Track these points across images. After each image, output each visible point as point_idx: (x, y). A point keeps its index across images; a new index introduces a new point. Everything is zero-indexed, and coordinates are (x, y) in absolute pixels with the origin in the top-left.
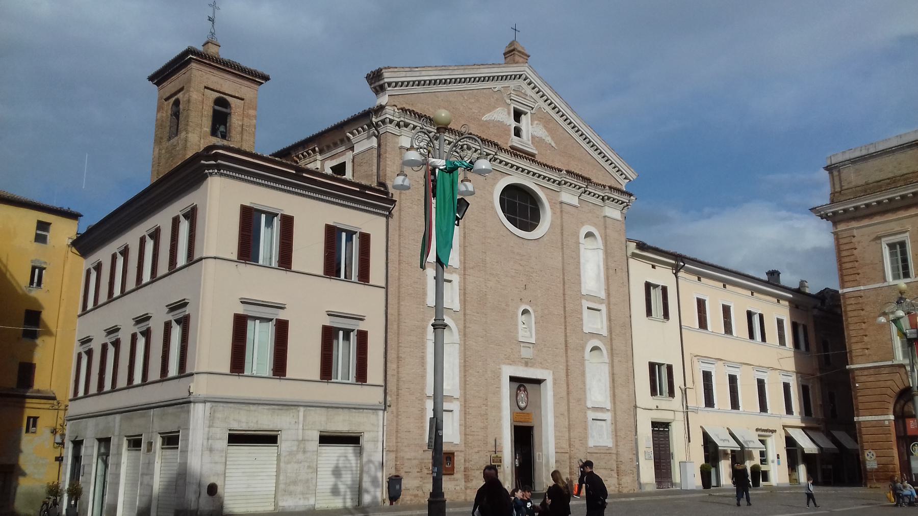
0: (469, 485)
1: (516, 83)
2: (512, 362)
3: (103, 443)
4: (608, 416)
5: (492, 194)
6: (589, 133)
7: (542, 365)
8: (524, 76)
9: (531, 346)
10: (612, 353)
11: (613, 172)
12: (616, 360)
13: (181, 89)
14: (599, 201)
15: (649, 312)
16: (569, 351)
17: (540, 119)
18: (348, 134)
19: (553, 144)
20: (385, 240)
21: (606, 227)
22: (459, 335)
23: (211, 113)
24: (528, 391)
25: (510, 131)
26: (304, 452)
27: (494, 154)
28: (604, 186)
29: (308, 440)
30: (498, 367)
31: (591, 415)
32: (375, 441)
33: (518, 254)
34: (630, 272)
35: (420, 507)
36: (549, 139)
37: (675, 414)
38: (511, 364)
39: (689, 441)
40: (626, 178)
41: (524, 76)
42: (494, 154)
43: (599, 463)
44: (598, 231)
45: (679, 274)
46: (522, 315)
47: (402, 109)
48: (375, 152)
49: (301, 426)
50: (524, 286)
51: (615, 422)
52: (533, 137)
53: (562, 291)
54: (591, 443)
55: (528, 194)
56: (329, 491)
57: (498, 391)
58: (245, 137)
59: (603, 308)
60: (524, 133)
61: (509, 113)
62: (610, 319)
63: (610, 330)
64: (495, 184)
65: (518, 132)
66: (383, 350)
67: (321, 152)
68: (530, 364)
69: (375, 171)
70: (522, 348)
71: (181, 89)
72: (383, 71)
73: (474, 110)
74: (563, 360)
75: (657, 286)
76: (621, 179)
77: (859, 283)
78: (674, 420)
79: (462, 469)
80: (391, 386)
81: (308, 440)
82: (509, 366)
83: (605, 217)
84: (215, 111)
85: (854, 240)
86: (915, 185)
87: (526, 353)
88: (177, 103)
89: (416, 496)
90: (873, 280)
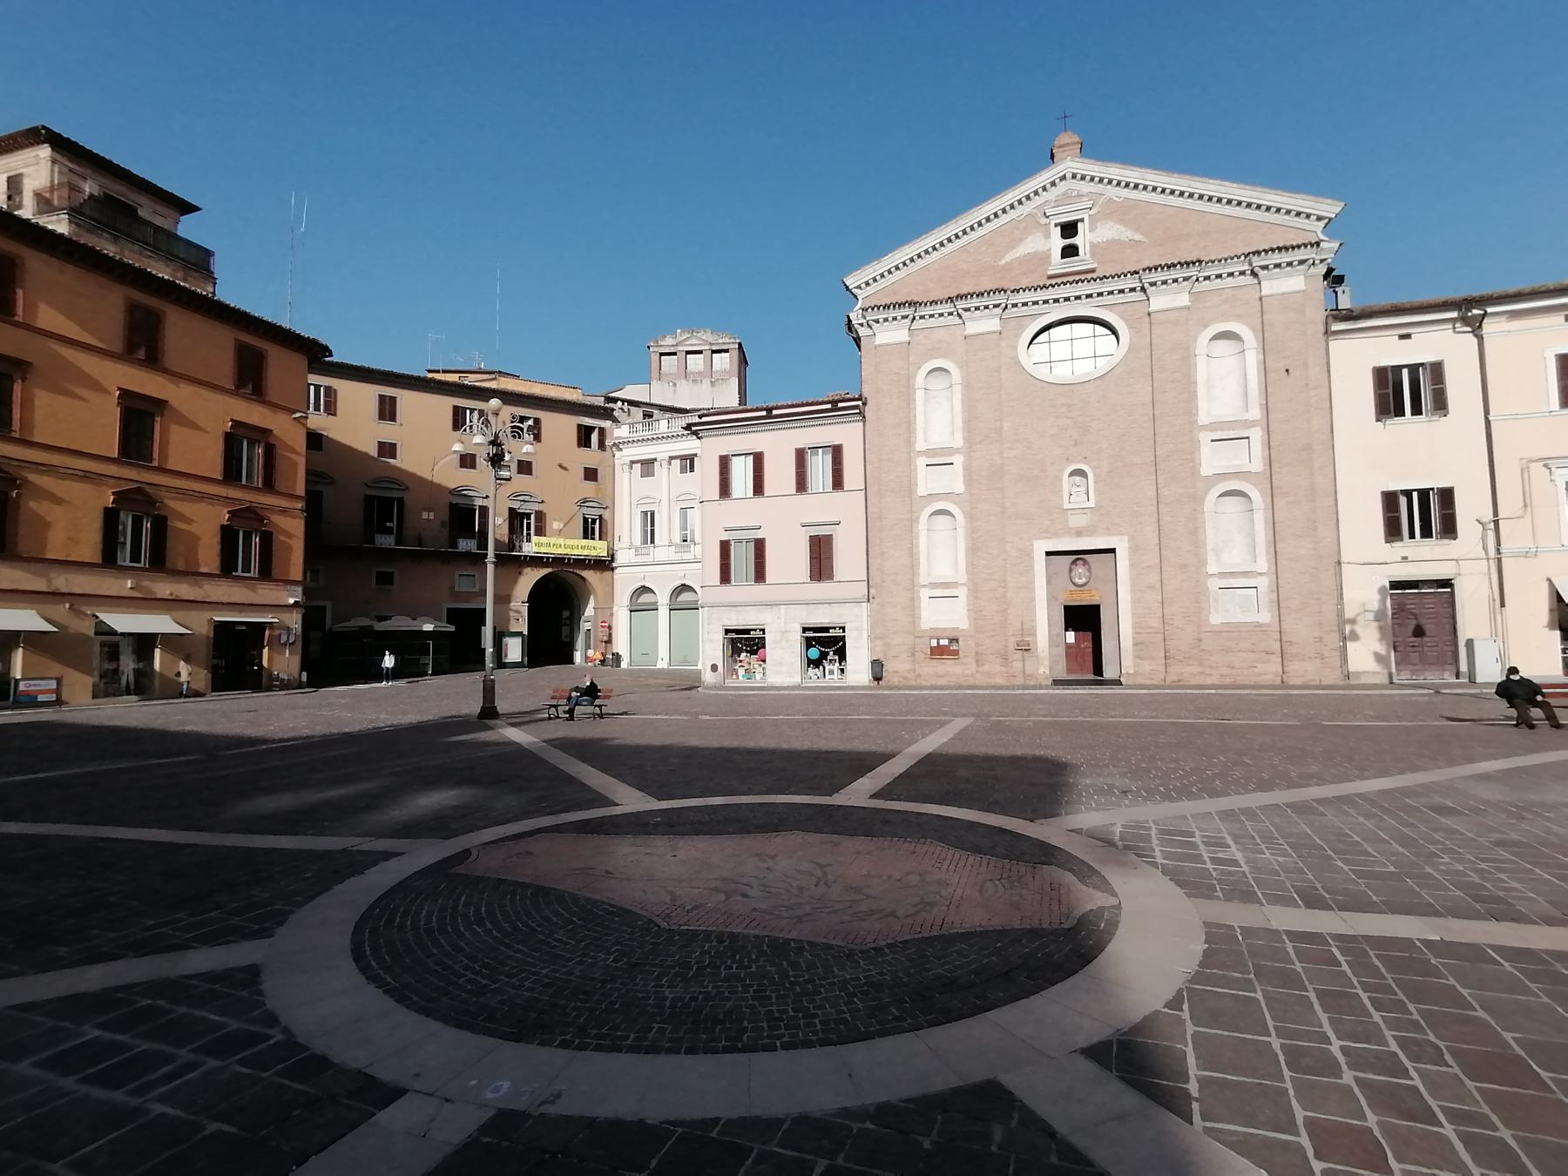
0: (981, 669)
2: (1047, 534)
6: (16, 717)
7: (1109, 532)
11: (1291, 220)
22: (965, 518)
24: (1091, 564)
26: (787, 641)
27: (1005, 301)
29: (790, 631)
30: (1028, 544)
31: (1214, 584)
32: (859, 629)
33: (1063, 405)
37: (1458, 564)
38: (1050, 538)
39: (1503, 605)
42: (1005, 301)
44: (1244, 324)
46: (1069, 476)
49: (783, 621)
50: (1074, 443)
54: (1216, 619)
57: (1030, 569)
64: (1019, 335)
65: (1070, 251)
70: (1069, 516)
73: (985, 260)
74: (1154, 519)
79: (974, 654)
81: (790, 631)
86: (132, 706)
87: (1076, 521)
89: (906, 678)
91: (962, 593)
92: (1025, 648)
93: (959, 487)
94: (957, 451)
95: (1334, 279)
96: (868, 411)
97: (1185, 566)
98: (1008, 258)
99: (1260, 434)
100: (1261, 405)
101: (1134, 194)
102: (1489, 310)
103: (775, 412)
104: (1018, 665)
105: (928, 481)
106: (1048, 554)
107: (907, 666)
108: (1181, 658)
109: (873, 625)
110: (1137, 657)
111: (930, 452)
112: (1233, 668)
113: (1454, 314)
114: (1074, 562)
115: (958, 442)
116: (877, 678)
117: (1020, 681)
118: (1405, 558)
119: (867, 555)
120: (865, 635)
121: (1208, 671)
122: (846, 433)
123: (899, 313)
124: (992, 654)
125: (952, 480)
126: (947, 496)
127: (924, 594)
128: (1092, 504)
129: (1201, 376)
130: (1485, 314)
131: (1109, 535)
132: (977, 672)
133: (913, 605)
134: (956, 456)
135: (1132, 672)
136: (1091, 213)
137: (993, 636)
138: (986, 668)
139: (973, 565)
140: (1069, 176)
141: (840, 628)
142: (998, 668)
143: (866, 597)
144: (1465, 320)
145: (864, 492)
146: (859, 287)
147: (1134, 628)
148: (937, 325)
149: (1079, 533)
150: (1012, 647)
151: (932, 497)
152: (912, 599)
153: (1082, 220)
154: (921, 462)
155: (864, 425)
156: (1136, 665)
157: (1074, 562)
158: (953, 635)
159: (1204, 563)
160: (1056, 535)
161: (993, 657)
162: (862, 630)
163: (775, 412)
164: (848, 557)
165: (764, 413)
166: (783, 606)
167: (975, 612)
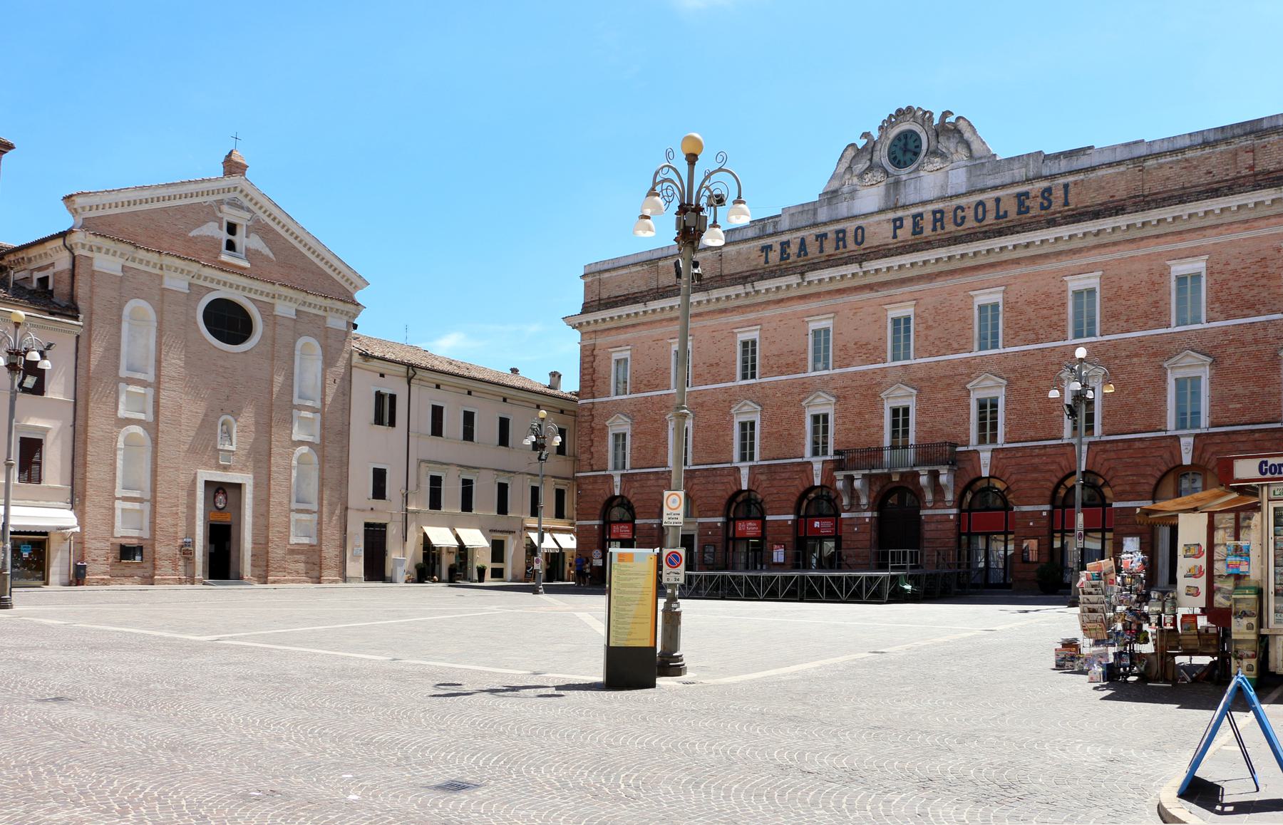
8: (239, 189)
12: (327, 466)
25: (220, 244)
33: (222, 366)
34: (353, 380)
35: (1218, 560)
36: (266, 251)
41: (239, 189)
56: (868, 543)
61: (221, 228)
63: (323, 438)
98: (193, 234)
146: (83, 208)
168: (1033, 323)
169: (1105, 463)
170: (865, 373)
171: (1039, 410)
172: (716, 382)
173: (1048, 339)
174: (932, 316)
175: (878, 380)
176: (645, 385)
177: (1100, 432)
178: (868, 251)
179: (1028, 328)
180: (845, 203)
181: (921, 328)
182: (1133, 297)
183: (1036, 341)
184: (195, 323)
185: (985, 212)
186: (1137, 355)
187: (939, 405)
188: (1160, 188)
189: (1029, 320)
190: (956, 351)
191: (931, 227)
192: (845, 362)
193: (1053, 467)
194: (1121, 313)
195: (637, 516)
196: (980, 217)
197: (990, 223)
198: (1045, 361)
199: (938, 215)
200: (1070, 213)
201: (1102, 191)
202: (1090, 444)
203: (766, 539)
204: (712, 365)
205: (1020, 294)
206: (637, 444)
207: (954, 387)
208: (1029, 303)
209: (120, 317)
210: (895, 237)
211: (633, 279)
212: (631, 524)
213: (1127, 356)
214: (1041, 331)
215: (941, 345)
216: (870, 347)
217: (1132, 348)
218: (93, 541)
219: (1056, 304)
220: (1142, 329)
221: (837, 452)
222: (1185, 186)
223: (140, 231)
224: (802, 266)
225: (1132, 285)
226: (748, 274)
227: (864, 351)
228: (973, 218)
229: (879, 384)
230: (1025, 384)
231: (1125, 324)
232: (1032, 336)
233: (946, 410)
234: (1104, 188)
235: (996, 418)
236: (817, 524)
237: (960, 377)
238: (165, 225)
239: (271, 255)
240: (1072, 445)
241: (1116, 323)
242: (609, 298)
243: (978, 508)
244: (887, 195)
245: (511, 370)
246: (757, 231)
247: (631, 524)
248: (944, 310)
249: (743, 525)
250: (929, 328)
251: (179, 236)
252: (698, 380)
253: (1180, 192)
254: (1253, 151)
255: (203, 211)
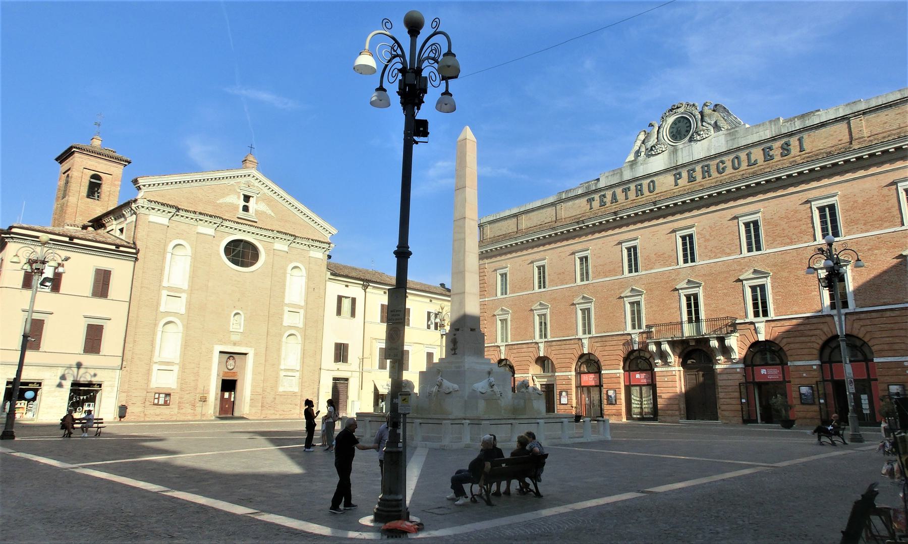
0: (181, 411)
1: (247, 179)
2: (221, 342)
3: (639, 411)
4: (297, 374)
5: (219, 246)
7: (247, 345)
8: (252, 176)
9: (239, 334)
10: (305, 337)
13: (69, 169)
14: (306, 248)
15: (339, 312)
16: (269, 337)
17: (263, 200)
18: (124, 212)
19: (273, 214)
20: (132, 275)
21: (309, 263)
23: (87, 184)
25: (238, 208)
28: (309, 239)
31: (282, 373)
36: (269, 212)
38: (222, 344)
39: (362, 389)
40: (330, 233)
43: (286, 401)
45: (367, 290)
47: (148, 201)
48: (134, 224)
51: (302, 378)
52: (256, 211)
53: (268, 302)
55: (248, 243)
57: (210, 359)
58: (111, 198)
59: (302, 311)
60: (251, 209)
61: (239, 198)
62: (306, 318)
63: (305, 324)
64: (222, 240)
65: (246, 209)
66: (124, 336)
67: (115, 219)
68: (237, 345)
69: (133, 235)
71: (69, 169)
72: (138, 179)
75: (346, 297)
76: (326, 233)
77: (485, 296)
78: (351, 377)
80: (127, 356)
82: (221, 346)
83: (310, 257)
84: (91, 183)
85: (485, 270)
87: (235, 338)
88: (68, 176)
90: (491, 296)
91: (176, 368)
92: (204, 400)
93: (183, 311)
94: (184, 291)
95: (329, 257)
96: (139, 256)
97: (274, 365)
98: (221, 201)
99: (303, 312)
100: (305, 300)
101: (275, 196)
102: (370, 284)
103: (76, 241)
104: (199, 410)
105: (167, 304)
106: (221, 352)
107: (140, 409)
108: (267, 406)
109: (122, 383)
110: (250, 406)
111: (169, 288)
112: (284, 411)
113: (362, 283)
114: (229, 358)
115: (185, 286)
116: (122, 416)
117: (198, 417)
118: (338, 369)
119: (125, 341)
120: (116, 389)
121: (276, 413)
122: (120, 269)
123: (167, 209)
124: (187, 403)
125: (179, 306)
126: (175, 314)
127: (155, 367)
128: (242, 331)
129: (288, 283)
130: (369, 285)
131: (247, 347)
132: (178, 413)
133: (149, 372)
134: (184, 294)
135: (248, 413)
136: (257, 196)
137: (189, 393)
138: (184, 411)
139: (184, 354)
140: (252, 176)
141: (37, 383)
142: (190, 411)
143: (120, 366)
144: (363, 285)
145: (128, 303)
146: (144, 186)
147: (251, 392)
148: (182, 222)
149: (235, 344)
150: (198, 399)
151: (168, 313)
152: (149, 370)
153: (253, 197)
154: (164, 293)
155: (135, 265)
156: (250, 410)
157: (229, 358)
158: (167, 392)
159: (279, 364)
160: (225, 343)
161: (188, 405)
162: (114, 386)
163: (76, 241)
164: (111, 341)
165: (67, 239)
166: (59, 368)
167: (182, 380)
168: (786, 232)
169: (862, 329)
170: (663, 273)
171: (799, 292)
172: (562, 284)
173: (799, 241)
174: (709, 233)
175: (673, 277)
176: (518, 288)
177: (854, 305)
178: (659, 195)
179: (783, 235)
180: (642, 166)
181: (702, 240)
182: (868, 207)
183: (791, 243)
184: (219, 254)
185: (739, 164)
186: (878, 248)
187: (720, 292)
188: (879, 130)
189: (783, 230)
190: (729, 255)
191: (701, 176)
192: (649, 267)
193: (818, 332)
194: (859, 219)
195: (516, 372)
196: (736, 161)
197: (745, 168)
198: (800, 257)
199: (706, 168)
200: (807, 155)
201: (831, 138)
202: (846, 314)
203: (602, 386)
204: (560, 274)
205: (773, 213)
206: (514, 326)
207: (730, 279)
208: (781, 218)
209: (165, 250)
210: (676, 185)
211: (509, 224)
212: (598, 374)
213: (869, 250)
214: (794, 237)
215: (717, 251)
216: (665, 255)
217: (872, 243)
218: (134, 391)
219: (804, 217)
220: (878, 228)
221: (647, 326)
222: (901, 126)
223: (183, 200)
224: (615, 208)
225: (865, 199)
226: (580, 216)
227: (662, 259)
228: (731, 167)
229: (675, 280)
230: (785, 274)
231: (863, 227)
232: (788, 241)
233: (725, 295)
234: (832, 135)
235: (821, 216)
236: (763, 371)
237: (734, 272)
238: (201, 196)
239: (273, 214)
240: (831, 316)
241: (856, 226)
242: (494, 237)
243: (758, 363)
244: (670, 158)
245: (440, 284)
246: (585, 189)
247: (598, 374)
248: (717, 228)
249: (587, 377)
250: (707, 240)
251: (210, 203)
252: (551, 284)
253: (898, 131)
254: (809, 267)
255: (227, 189)
